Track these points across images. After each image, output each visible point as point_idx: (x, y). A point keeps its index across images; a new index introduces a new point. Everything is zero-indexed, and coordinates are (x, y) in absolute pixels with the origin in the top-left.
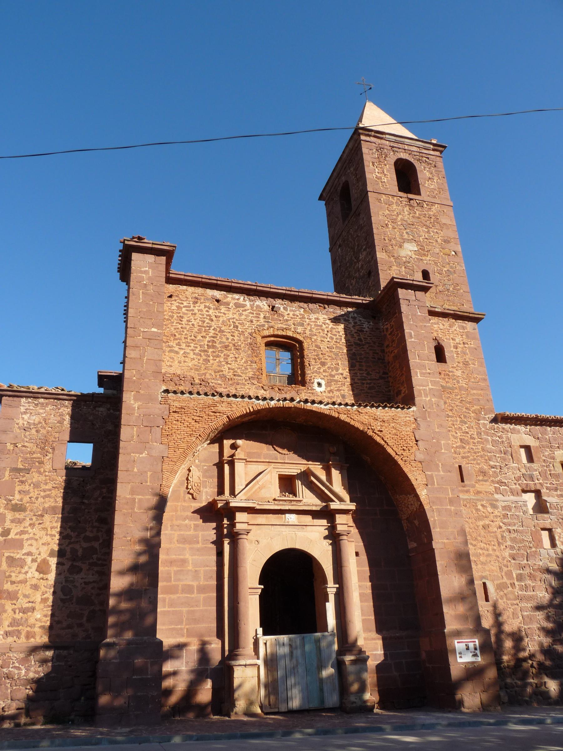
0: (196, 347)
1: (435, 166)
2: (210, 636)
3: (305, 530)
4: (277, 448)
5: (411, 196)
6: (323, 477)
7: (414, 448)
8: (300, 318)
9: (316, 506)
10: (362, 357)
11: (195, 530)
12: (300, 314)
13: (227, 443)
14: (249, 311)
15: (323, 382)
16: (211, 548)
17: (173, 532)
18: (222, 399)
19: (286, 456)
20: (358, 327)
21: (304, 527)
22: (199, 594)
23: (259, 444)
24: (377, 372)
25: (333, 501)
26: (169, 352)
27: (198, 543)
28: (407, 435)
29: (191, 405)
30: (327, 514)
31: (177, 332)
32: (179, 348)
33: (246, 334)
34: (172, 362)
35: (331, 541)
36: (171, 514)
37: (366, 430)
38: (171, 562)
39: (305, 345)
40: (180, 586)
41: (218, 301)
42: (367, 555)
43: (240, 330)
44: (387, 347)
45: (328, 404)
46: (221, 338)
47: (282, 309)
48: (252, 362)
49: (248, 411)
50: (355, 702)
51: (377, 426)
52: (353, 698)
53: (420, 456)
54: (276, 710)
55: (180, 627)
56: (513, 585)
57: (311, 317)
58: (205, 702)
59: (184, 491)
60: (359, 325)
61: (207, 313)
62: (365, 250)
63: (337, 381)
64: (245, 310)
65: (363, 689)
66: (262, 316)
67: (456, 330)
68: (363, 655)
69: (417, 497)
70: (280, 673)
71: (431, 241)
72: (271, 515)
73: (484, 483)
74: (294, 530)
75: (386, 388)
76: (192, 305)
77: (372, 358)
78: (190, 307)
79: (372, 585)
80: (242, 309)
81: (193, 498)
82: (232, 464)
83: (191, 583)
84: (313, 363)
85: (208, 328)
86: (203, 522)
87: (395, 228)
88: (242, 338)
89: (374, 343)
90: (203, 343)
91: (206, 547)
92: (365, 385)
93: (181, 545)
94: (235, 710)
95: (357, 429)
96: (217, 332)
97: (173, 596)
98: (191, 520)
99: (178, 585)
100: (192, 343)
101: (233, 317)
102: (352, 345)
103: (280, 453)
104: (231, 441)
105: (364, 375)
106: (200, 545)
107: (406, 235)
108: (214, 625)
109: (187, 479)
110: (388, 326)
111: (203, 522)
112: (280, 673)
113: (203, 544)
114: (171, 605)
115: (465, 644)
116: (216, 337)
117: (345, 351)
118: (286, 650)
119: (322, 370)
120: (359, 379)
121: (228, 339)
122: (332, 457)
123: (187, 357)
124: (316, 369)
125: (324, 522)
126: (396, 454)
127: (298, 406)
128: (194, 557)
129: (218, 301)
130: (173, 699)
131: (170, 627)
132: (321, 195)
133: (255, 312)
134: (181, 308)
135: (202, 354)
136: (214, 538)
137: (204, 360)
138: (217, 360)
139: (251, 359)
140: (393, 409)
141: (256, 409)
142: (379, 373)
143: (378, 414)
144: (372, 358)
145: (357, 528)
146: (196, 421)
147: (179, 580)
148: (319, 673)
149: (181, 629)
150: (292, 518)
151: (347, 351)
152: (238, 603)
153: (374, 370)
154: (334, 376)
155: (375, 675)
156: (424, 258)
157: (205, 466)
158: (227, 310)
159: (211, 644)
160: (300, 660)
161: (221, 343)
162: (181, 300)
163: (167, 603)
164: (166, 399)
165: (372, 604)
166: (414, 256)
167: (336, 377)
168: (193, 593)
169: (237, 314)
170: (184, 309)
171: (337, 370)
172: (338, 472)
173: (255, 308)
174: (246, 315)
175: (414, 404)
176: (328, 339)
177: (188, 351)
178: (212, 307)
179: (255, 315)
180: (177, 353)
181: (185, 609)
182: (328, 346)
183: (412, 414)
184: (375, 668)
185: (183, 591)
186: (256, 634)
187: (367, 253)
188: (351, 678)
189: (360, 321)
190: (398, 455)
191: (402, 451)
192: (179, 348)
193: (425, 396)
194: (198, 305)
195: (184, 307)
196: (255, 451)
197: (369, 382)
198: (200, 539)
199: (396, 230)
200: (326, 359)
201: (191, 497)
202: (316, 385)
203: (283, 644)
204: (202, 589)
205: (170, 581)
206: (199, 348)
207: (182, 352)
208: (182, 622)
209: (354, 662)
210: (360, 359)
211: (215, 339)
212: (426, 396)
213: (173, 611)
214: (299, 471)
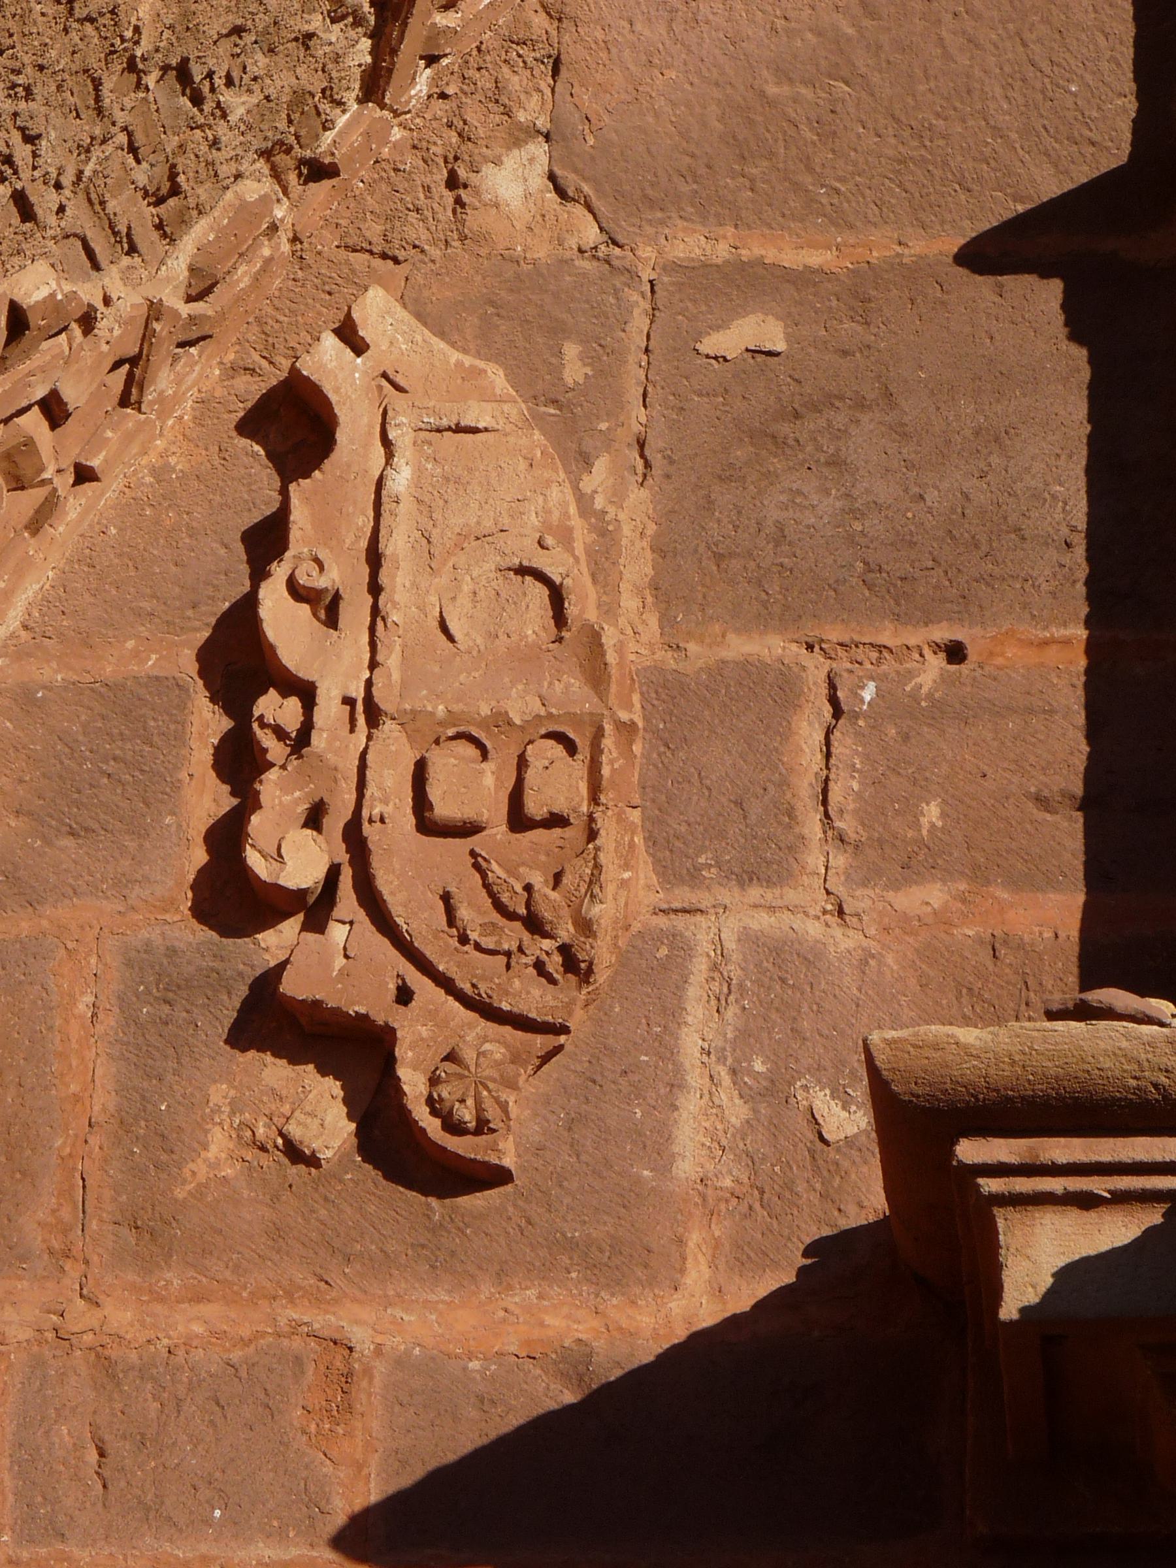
59: (160, 982)
81: (394, 1146)
109: (238, 662)
157: (747, 283)
201: (322, 1112)
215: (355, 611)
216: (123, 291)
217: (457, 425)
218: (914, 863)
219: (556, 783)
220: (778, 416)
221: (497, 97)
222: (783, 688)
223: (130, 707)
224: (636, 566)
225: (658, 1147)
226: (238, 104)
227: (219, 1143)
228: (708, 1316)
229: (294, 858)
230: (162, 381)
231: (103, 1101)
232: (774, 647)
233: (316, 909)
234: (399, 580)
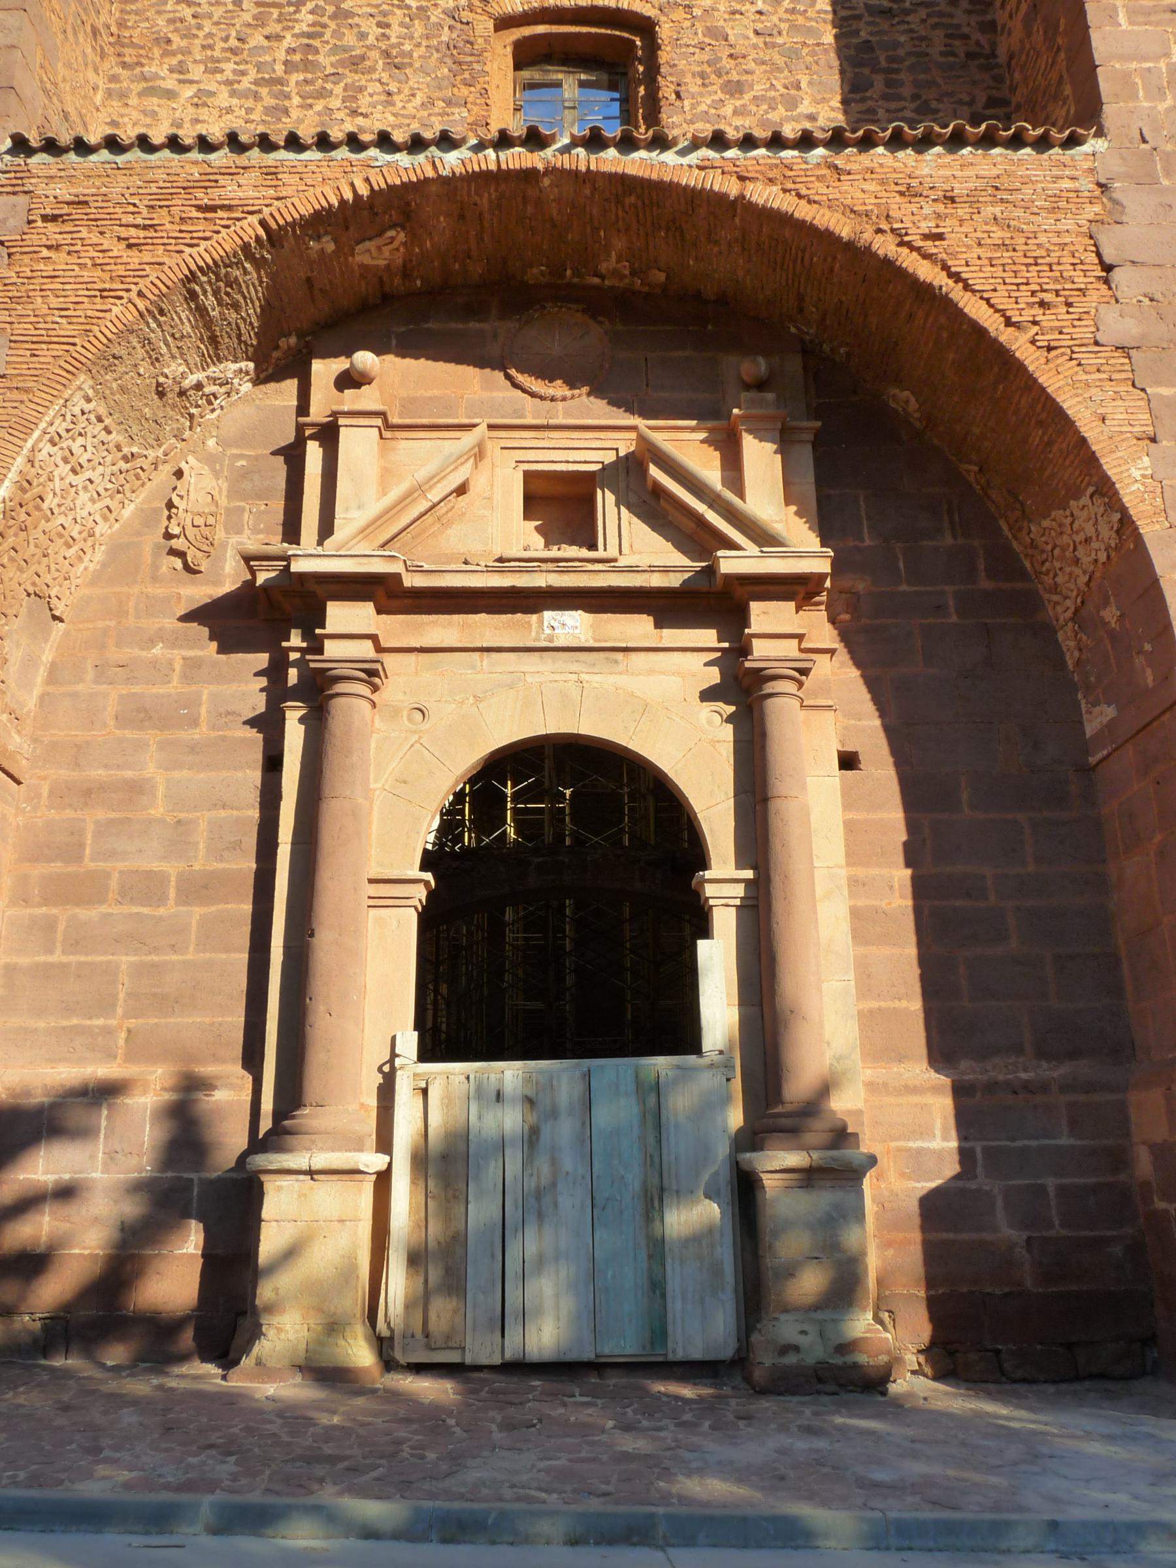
0: (243, 73)
2: (216, 1059)
3: (621, 667)
4: (520, 378)
6: (711, 472)
7: (1093, 296)
9: (666, 570)
10: (901, 52)
13: (324, 370)
16: (243, 740)
17: (103, 688)
18: (242, 160)
19: (560, 405)
21: (619, 656)
22: (186, 903)
23: (451, 367)
25: (732, 545)
26: (140, 95)
27: (194, 722)
29: (115, 192)
30: (715, 603)
31: (176, 30)
32: (180, 81)
33: (435, 16)
34: (148, 126)
35: (732, 709)
36: (100, 624)
37: (868, 236)
39: (664, 32)
40: (116, 876)
42: (897, 765)
45: (695, 144)
46: (337, 34)
48: (449, 103)
49: (348, 195)
50: (796, 1348)
51: (919, 219)
52: (788, 1329)
53: (1118, 325)
54: (453, 1357)
55: (101, 1022)
58: (170, 1307)
59: (158, 546)
65: (845, 1289)
68: (847, 1153)
69: (1106, 489)
70: (481, 1212)
72: (483, 615)
74: (575, 667)
79: (914, 879)
81: (187, 568)
82: (329, 435)
83: (156, 866)
84: (694, 89)
85: (292, 9)
86: (220, 651)
88: (418, 28)
90: (268, 58)
91: (224, 739)
93: (129, 734)
94: (256, 1350)
95: (828, 236)
96: (325, 20)
97: (85, 913)
98: (173, 644)
99: (107, 875)
100: (229, 60)
102: (859, 17)
103: (533, 395)
104: (339, 365)
106: (200, 733)
108: (237, 1019)
109: (170, 505)
111: (220, 651)
112: (481, 1212)
113: (213, 728)
114: (74, 944)
116: (321, 35)
117: (829, 38)
118: (511, 1120)
119: (728, 110)
121: (363, 36)
122: (744, 395)
123: (205, 105)
124: (703, 107)
125: (708, 637)
126: (1008, 322)
127: (565, 162)
128: (177, 774)
130: (53, 1290)
131: (65, 1023)
135: (264, 91)
136: (259, 704)
137: (268, 110)
138: (318, 107)
140: (997, 151)
141: (379, 183)
142: (971, 103)
143: (926, 171)
144: (942, 54)
145: (858, 664)
146: (130, 246)
147: (112, 854)
148: (648, 1219)
149: (108, 1031)
150: (571, 625)
151: (836, 37)
152: (312, 935)
155: (916, 1236)
157: (242, 456)
159: (213, 1087)
160: (568, 1163)
161: (336, 49)
163: (59, 936)
164: (22, 175)
165: (912, 951)
168: (162, 900)
172: (770, 447)
177: (212, 87)
180: (170, 95)
181: (125, 960)
182: (759, 26)
183: (1087, 165)
184: (914, 1207)
185: (126, 894)
186: (394, 1055)
188: (789, 1245)
190: (1017, 325)
191: (1037, 311)
192: (180, 81)
193: (1148, 97)
196: (436, 392)
198: (203, 710)
200: (747, 72)
203: (499, 1096)
204: (196, 889)
205: (80, 858)
206: (253, 74)
207: (188, 92)
208: (113, 1006)
209: (809, 1177)
210: (891, 60)
211: (316, 43)
213: (80, 965)
214: (610, 457)
215: (185, 498)
216: (151, 454)
217: (760, 677)
218: (260, 532)
219: (211, 520)
220: (245, 474)
221: (210, 432)
222: (243, 509)
223: (156, 511)
224: (225, 493)
225: (223, 568)
226: (168, 428)
227: (164, 568)
228: (229, 590)
229: (175, 530)
230: (160, 467)
231: (149, 562)
232: (242, 504)
233: (178, 537)
234: (191, 494)
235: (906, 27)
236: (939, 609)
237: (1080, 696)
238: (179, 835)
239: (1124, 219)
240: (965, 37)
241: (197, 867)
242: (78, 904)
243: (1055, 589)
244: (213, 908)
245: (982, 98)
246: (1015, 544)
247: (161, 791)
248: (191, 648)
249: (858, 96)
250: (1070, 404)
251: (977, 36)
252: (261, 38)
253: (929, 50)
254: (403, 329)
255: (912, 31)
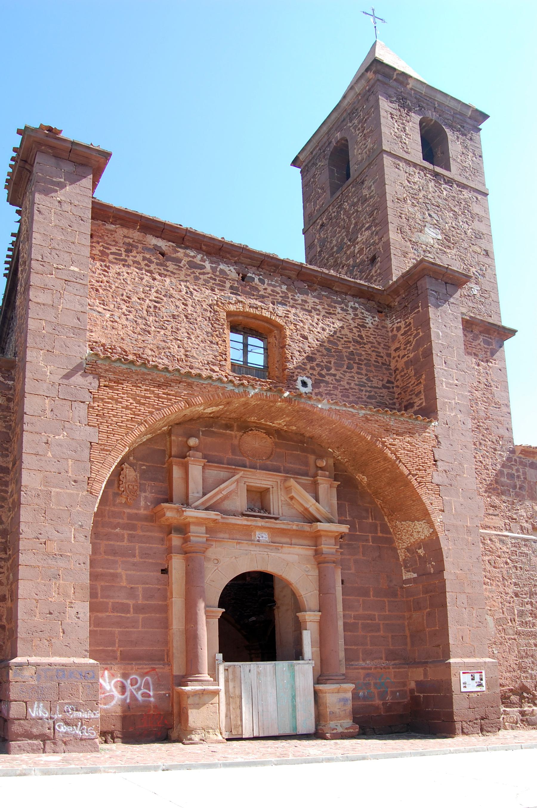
1: (471, 138)
3: (280, 551)
5: (438, 169)
8: (280, 297)
11: (129, 541)
12: (282, 291)
14: (209, 276)
15: (309, 382)
20: (359, 320)
22: (137, 613)
24: (379, 379)
28: (425, 453)
31: (100, 286)
38: (97, 576)
40: (110, 604)
41: (163, 254)
43: (196, 299)
44: (395, 350)
47: (256, 280)
53: (437, 479)
55: (111, 648)
56: (513, 620)
57: (296, 298)
60: (360, 318)
61: (147, 268)
62: (368, 228)
63: (327, 383)
64: (204, 274)
66: (228, 285)
67: (479, 344)
71: (458, 231)
73: (494, 517)
74: (266, 550)
75: (390, 399)
76: (124, 254)
77: (375, 361)
78: (121, 255)
80: (199, 271)
83: (125, 601)
85: (148, 289)
87: (415, 206)
89: (379, 343)
91: (145, 562)
92: (364, 393)
101: (186, 279)
102: (350, 342)
105: (364, 380)
106: (137, 559)
107: (429, 218)
110: (402, 324)
113: (141, 558)
115: (470, 674)
119: (308, 367)
120: (356, 385)
128: (129, 572)
129: (163, 254)
132: (297, 158)
133: (217, 279)
134: (107, 255)
139: (210, 338)
142: (382, 381)
143: (392, 424)
147: (108, 597)
153: (375, 376)
154: (324, 377)
156: (448, 251)
158: (176, 269)
162: (108, 244)
166: (436, 246)
167: (327, 377)
168: (128, 612)
169: (192, 276)
170: (111, 257)
171: (329, 369)
173: (218, 273)
174: (204, 280)
175: (436, 419)
176: (319, 330)
178: (155, 261)
179: (217, 282)
181: (117, 630)
187: (372, 234)
189: (363, 313)
193: (449, 411)
194: (133, 254)
195: (112, 253)
197: (369, 389)
198: (137, 551)
199: (416, 208)
202: (299, 383)
210: (360, 360)
212: (452, 410)
213: (100, 631)
235: (364, 349)
236: (367, 540)
237: (403, 568)
238: (132, 593)
239: (441, 447)
240: (382, 357)
241: (140, 602)
242: (97, 612)
243: (401, 539)
244: (147, 615)
245: (386, 380)
246: (388, 524)
247: (124, 577)
248: (130, 531)
249: (349, 371)
250: (424, 498)
251: (385, 357)
252: (136, 298)
253: (371, 359)
254: (204, 429)
255: (366, 351)
